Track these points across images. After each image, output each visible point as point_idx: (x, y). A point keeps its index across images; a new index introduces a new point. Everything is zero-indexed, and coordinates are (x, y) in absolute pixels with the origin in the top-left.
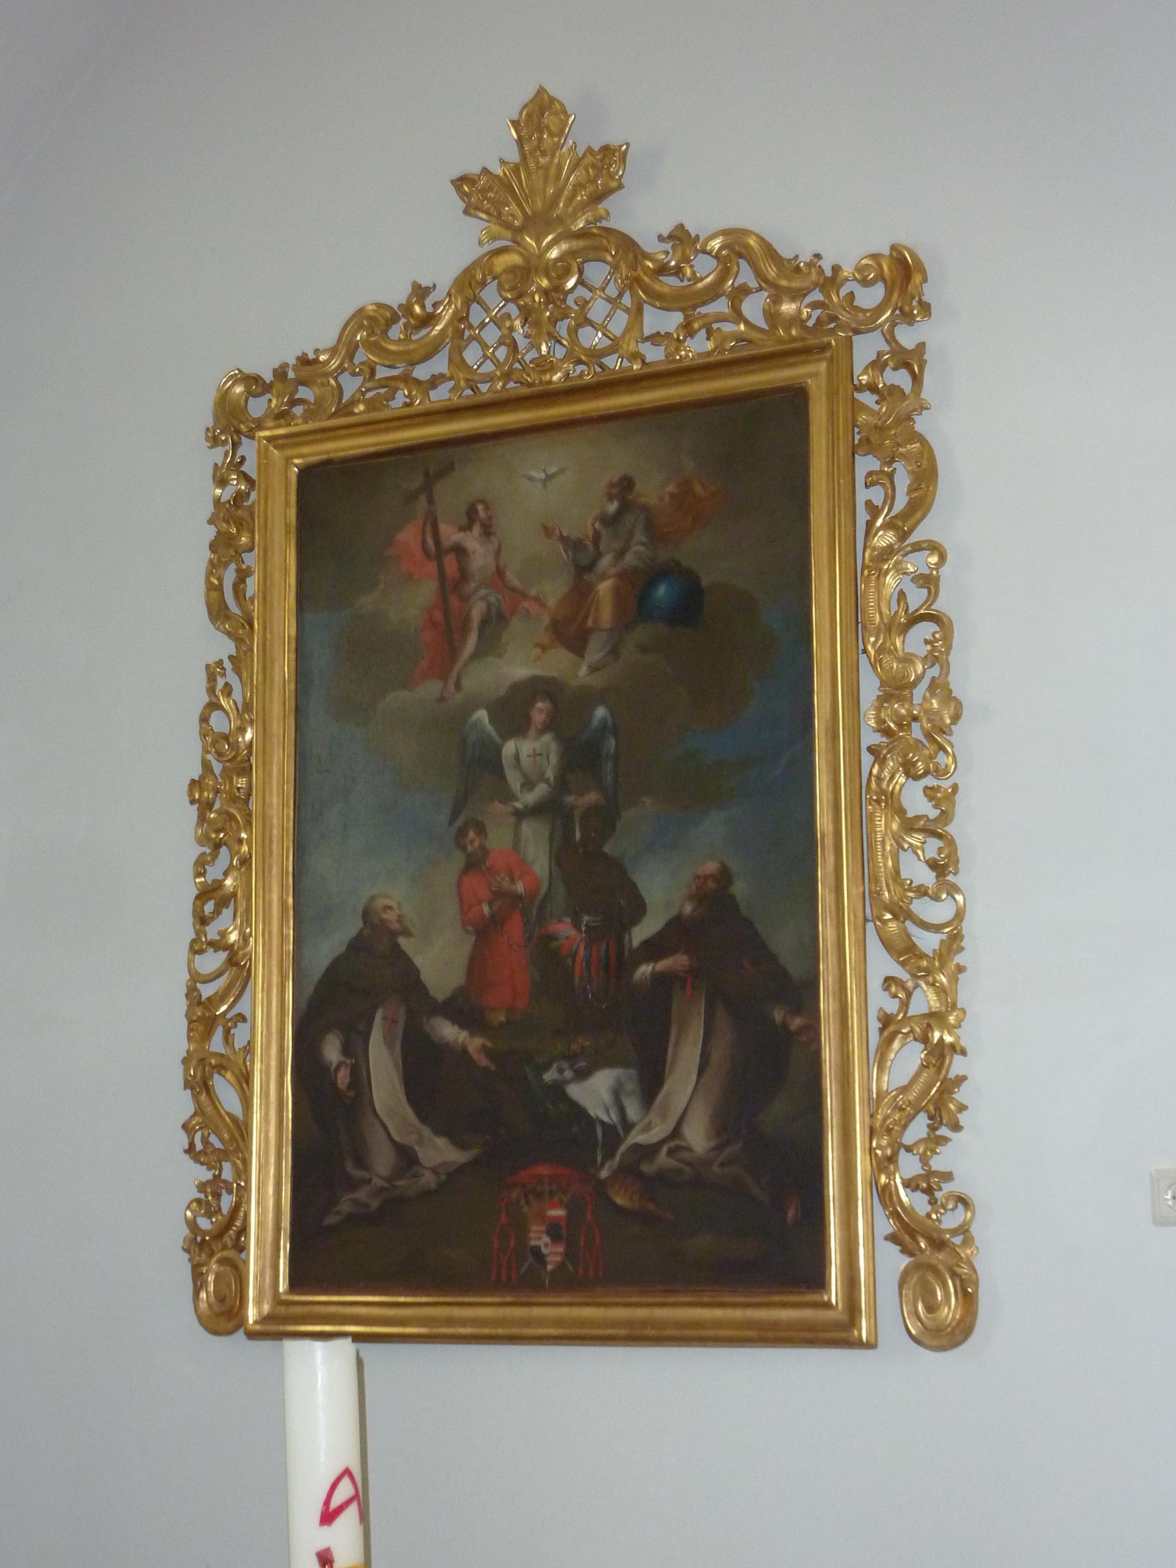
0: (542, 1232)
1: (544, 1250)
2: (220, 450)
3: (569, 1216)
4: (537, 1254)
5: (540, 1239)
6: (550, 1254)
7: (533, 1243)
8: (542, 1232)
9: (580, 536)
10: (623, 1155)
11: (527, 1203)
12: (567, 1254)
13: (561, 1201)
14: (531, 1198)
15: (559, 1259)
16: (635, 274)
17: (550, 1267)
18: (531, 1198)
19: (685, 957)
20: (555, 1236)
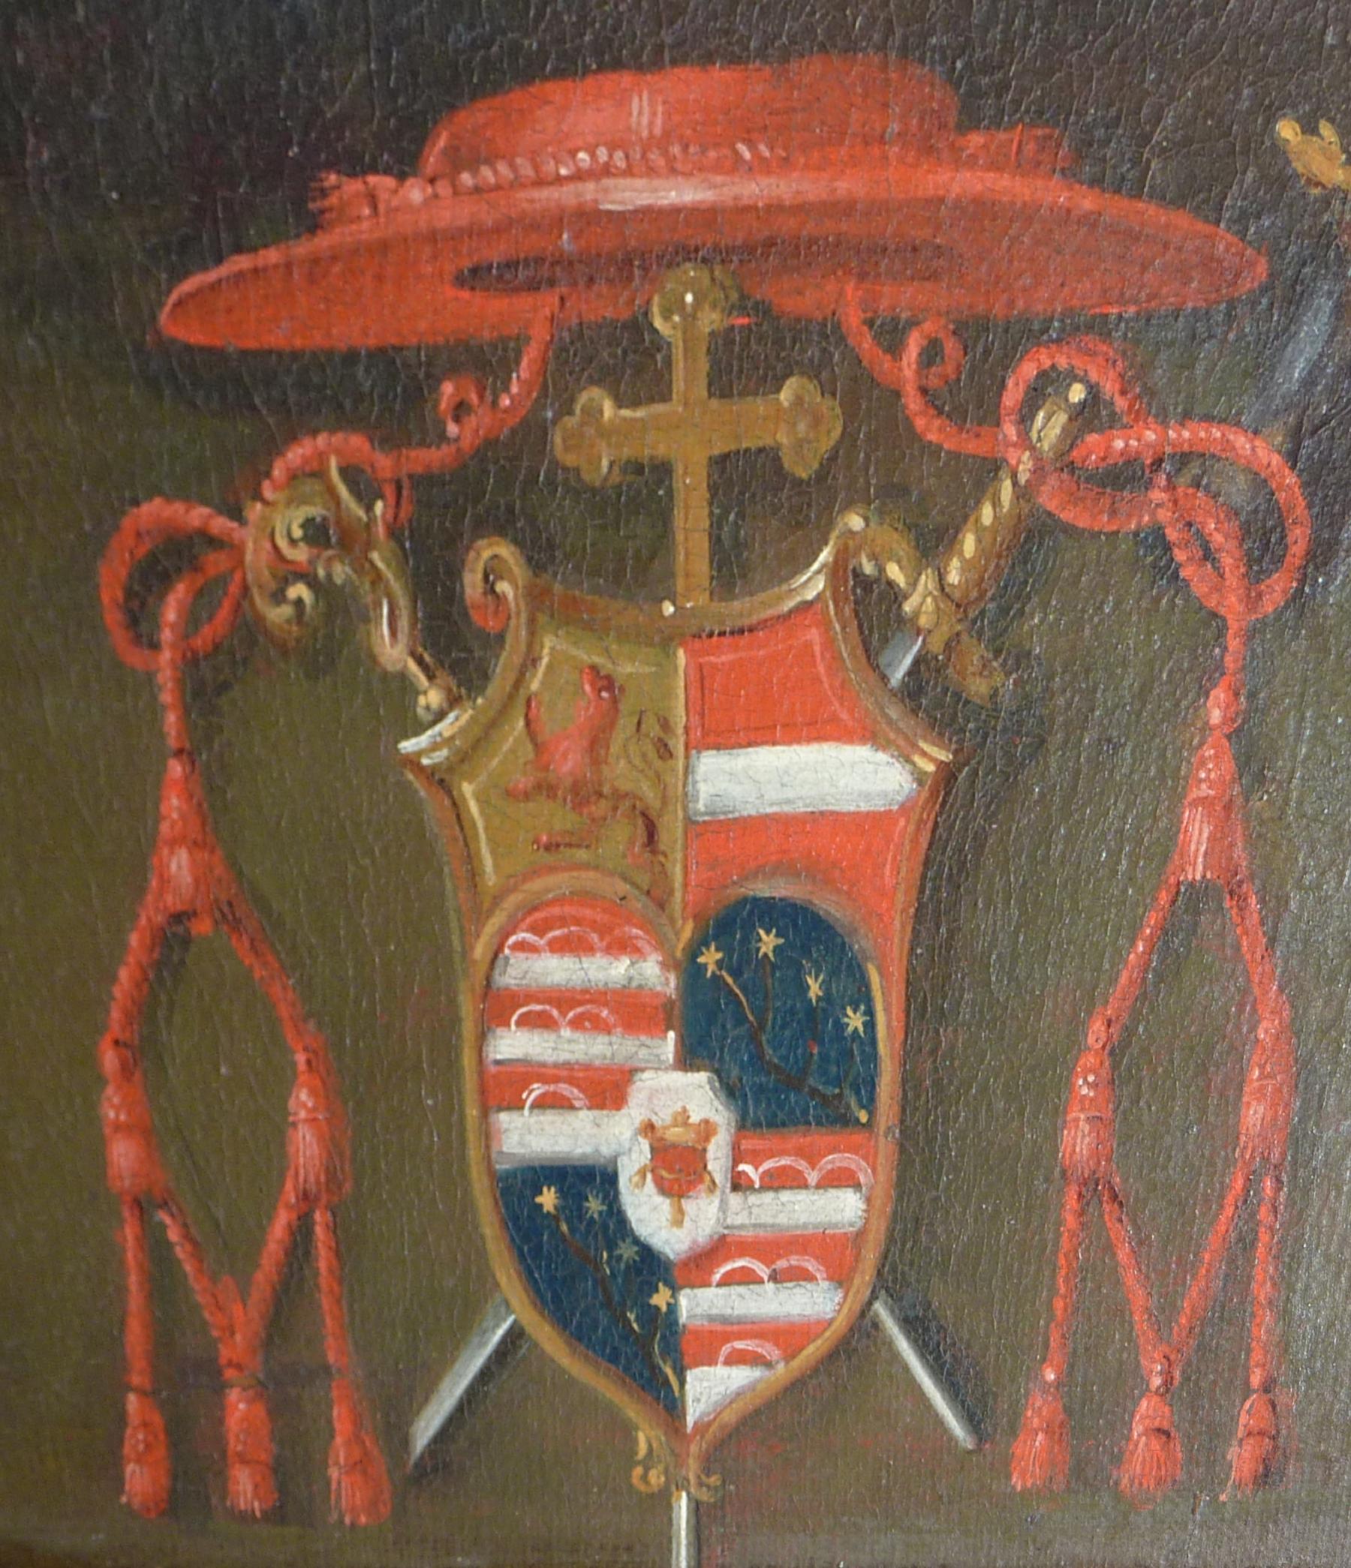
0: (631, 1011)
1: (650, 1216)
2: (293, 643)
3: (957, 835)
4: (578, 1250)
5: (603, 1090)
6: (700, 1265)
7: (529, 1135)
8: (631, 1011)
9: (675, 70)
10: (734, 1270)
11: (456, 646)
12: (905, 1262)
13: (872, 608)
14: (494, 569)
15: (815, 1302)
16: (634, 1113)
17: (710, 1388)
18: (494, 569)
19: (1076, 400)
20: (769, 1014)
